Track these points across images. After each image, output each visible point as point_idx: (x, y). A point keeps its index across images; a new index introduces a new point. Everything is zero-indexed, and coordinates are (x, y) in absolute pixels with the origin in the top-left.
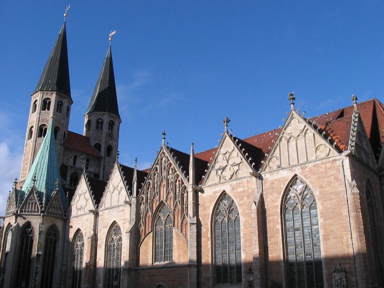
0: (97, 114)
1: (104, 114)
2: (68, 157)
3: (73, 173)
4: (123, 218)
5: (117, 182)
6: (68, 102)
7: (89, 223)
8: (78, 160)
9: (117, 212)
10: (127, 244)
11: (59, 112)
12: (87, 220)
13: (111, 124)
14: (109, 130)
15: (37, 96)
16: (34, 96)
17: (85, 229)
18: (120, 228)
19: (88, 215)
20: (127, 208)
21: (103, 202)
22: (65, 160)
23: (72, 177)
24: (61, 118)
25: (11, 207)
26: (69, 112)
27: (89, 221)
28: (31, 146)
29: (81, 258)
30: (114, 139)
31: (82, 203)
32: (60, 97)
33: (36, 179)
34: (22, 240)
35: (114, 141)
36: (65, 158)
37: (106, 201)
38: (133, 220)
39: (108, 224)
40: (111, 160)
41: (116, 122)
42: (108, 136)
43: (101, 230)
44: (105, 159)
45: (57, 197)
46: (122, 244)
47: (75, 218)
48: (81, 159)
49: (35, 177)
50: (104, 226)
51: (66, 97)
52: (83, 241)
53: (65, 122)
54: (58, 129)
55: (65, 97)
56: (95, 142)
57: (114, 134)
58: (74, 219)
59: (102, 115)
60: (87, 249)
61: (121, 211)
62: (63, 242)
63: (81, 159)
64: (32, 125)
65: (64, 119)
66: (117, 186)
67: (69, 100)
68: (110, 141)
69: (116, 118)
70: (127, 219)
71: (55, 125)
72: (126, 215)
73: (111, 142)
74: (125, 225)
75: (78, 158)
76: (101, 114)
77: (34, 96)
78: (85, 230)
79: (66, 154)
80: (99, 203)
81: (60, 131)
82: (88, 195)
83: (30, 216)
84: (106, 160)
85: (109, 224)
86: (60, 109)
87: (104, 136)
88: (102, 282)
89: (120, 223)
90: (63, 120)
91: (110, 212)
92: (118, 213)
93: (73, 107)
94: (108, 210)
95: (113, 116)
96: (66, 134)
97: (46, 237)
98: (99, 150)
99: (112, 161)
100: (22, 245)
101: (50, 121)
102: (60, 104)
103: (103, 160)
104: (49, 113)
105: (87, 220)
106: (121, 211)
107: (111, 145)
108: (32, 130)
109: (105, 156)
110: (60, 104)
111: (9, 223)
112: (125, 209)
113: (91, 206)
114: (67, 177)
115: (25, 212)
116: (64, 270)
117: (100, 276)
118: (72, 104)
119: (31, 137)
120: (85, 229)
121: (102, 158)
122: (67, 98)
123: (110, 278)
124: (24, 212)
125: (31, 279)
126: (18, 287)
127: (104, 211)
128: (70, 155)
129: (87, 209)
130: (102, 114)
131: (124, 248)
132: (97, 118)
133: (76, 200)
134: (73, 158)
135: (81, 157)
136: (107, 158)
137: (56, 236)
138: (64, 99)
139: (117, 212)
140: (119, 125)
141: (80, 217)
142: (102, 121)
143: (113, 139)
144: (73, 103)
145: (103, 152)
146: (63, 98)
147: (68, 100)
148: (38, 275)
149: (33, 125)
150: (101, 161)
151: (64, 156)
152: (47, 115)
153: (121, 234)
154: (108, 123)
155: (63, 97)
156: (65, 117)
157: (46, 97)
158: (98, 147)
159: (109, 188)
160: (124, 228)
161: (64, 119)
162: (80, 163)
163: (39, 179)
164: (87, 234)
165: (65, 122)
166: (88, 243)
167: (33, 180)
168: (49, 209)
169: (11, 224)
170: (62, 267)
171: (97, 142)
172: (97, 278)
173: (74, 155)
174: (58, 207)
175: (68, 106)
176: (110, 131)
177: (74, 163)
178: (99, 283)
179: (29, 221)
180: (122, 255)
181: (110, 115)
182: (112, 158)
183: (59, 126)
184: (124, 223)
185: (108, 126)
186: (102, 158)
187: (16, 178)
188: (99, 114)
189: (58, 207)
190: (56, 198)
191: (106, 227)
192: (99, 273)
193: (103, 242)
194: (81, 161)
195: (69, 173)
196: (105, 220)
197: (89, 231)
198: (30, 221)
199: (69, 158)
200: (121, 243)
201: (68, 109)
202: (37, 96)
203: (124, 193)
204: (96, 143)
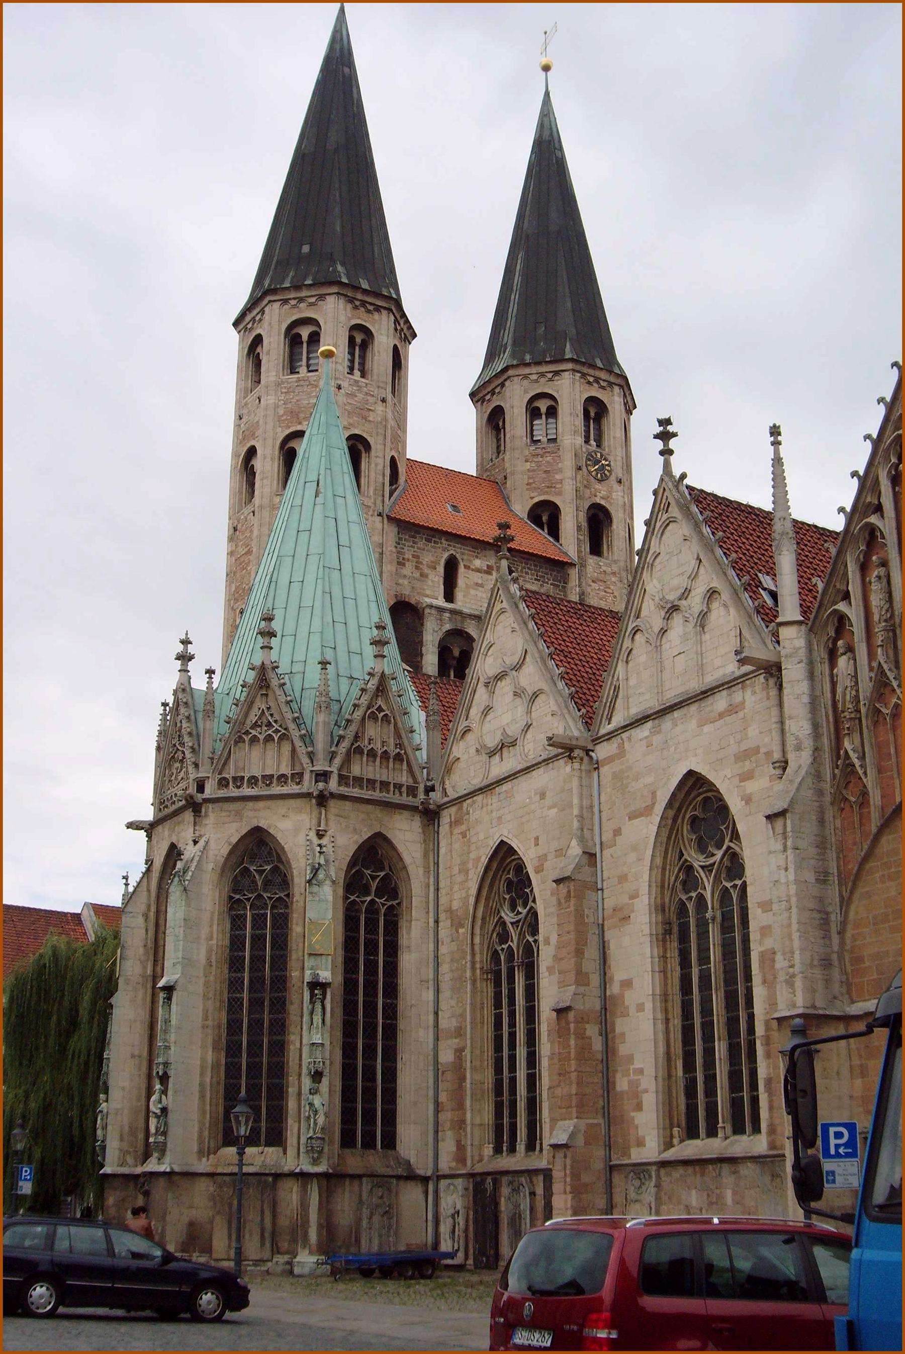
0: (525, 377)
1: (557, 373)
2: (417, 568)
3: (449, 633)
4: (733, 749)
5: (682, 574)
6: (396, 329)
7: (550, 808)
8: (463, 578)
9: (701, 725)
10: (783, 880)
11: (357, 373)
12: (543, 795)
13: (595, 412)
14: (587, 441)
15: (260, 320)
16: (245, 323)
17: (537, 839)
18: (724, 809)
19: (542, 770)
20: (754, 693)
21: (617, 689)
22: (406, 582)
23: (444, 652)
24: (371, 400)
25: (175, 771)
26: (403, 372)
27: (548, 801)
28: (251, 531)
29: (531, 992)
30: (613, 478)
31: (506, 719)
32: (356, 308)
33: (276, 625)
34: (237, 922)
35: (616, 486)
36: (408, 570)
37: (632, 682)
38: (798, 748)
39: (654, 793)
40: (609, 570)
41: (614, 401)
42: (584, 468)
43: (617, 832)
44: (583, 565)
45: (380, 702)
46: (749, 890)
47: (479, 798)
48: (478, 570)
49: (269, 619)
50: (632, 808)
51: (385, 308)
52: (530, 904)
53: (390, 415)
54: (361, 447)
55: (378, 309)
56: (532, 498)
57: (611, 458)
58: (474, 802)
59: (551, 380)
60: (554, 938)
61: (721, 716)
62: (431, 920)
63: (478, 570)
64: (248, 445)
65: (384, 400)
66: (686, 594)
67: (396, 321)
68: (598, 486)
69: (611, 384)
70: (763, 750)
71: (345, 428)
72: (753, 731)
73: (600, 494)
74: (753, 787)
75: (461, 569)
76: (542, 375)
77: (245, 323)
78: (537, 844)
79: (408, 555)
80: (596, 697)
81: (373, 453)
82: (532, 676)
83: (261, 804)
84: (590, 569)
85: (659, 793)
86: (362, 364)
87: (568, 463)
88: (650, 1100)
89: (725, 782)
90: (380, 408)
91: (659, 732)
92: (707, 728)
93: (415, 353)
94: (649, 724)
95: (597, 380)
96: (402, 469)
97: (346, 898)
98: (554, 532)
99: (614, 574)
100: (236, 943)
101: (472, 1278)
102: (358, 340)
103: (574, 573)
104: (318, 381)
105: (543, 795)
106: (721, 716)
107: (603, 502)
108: (253, 466)
109: (579, 551)
110: (358, 340)
111: (173, 846)
112: (743, 702)
113: (555, 718)
114: (422, 655)
115: (238, 787)
116: (446, 1056)
117: (641, 1071)
118: (413, 342)
119: (253, 497)
120: (537, 839)
121: (572, 565)
122: (389, 310)
123: (694, 1081)
124: (234, 782)
125: (292, 1104)
126: (832, 1348)
127: (624, 735)
128: (427, 558)
129: (534, 747)
130: (550, 375)
131: (766, 906)
132: (526, 392)
133: (473, 711)
134: (441, 569)
135: (477, 563)
136: (592, 560)
137: (394, 893)
138: (376, 316)
139: (701, 725)
140: (629, 419)
141: (505, 787)
142: (550, 403)
143: (607, 478)
144: (414, 335)
145: (571, 539)
146: (369, 311)
147: (392, 318)
148: (325, 1081)
149: (252, 443)
150: (565, 580)
151: (401, 564)
152: (309, 389)
153: (736, 836)
154: (580, 410)
155: (371, 308)
156: (389, 396)
157: (294, 318)
158: (546, 516)
159: (643, 614)
160: (748, 800)
161: (384, 400)
162: (473, 592)
163: (289, 629)
164: (546, 865)
165: (390, 415)
166: (560, 903)
167: (262, 633)
168: (347, 761)
169: (181, 845)
170: (437, 1039)
171: (542, 498)
172: (622, 1084)
173: (446, 555)
174: (393, 751)
175: (395, 348)
176: (593, 442)
177: (449, 596)
178: (639, 1107)
179: (260, 825)
180: (752, 946)
181: (584, 375)
182: (615, 562)
183: (365, 435)
184: (747, 777)
185: (580, 421)
186: (572, 565)
187: (184, 637)
188: (534, 377)
189: (393, 751)
190: (380, 709)
191: (647, 811)
192: (630, 1059)
193: (637, 890)
194: (480, 582)
195: (431, 636)
196: (637, 779)
197: (555, 845)
198: (263, 824)
199: (426, 570)
200: (739, 882)
201: (398, 362)
202: (260, 320)
203: (726, 619)
204: (536, 500)
